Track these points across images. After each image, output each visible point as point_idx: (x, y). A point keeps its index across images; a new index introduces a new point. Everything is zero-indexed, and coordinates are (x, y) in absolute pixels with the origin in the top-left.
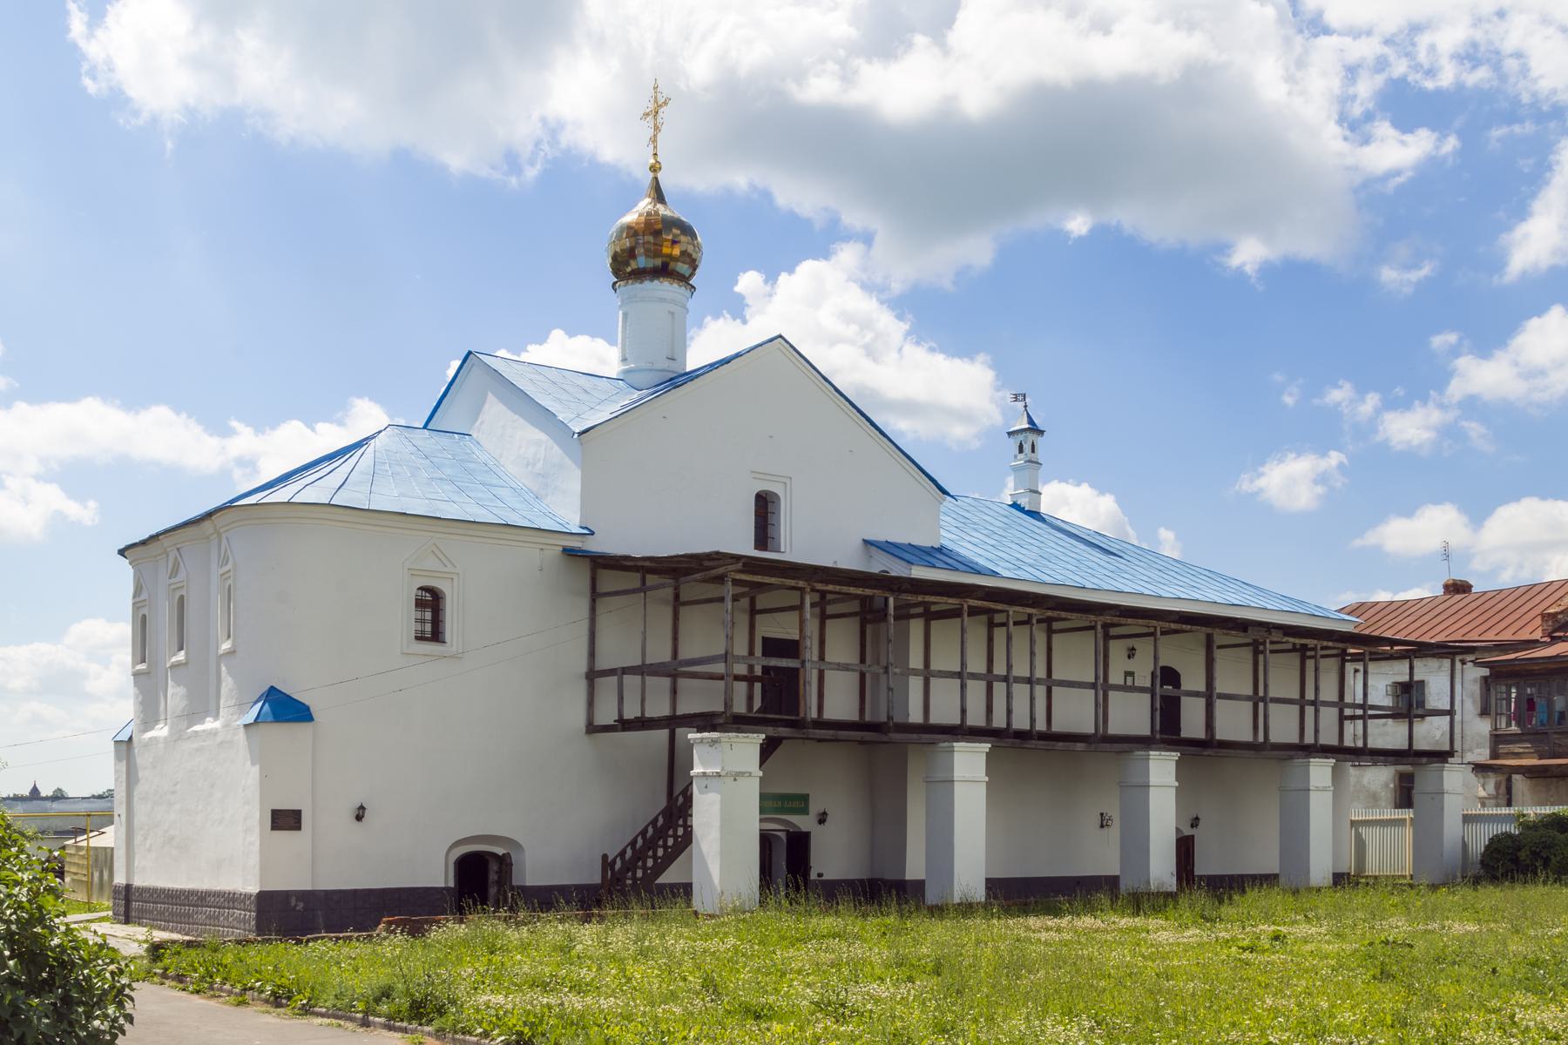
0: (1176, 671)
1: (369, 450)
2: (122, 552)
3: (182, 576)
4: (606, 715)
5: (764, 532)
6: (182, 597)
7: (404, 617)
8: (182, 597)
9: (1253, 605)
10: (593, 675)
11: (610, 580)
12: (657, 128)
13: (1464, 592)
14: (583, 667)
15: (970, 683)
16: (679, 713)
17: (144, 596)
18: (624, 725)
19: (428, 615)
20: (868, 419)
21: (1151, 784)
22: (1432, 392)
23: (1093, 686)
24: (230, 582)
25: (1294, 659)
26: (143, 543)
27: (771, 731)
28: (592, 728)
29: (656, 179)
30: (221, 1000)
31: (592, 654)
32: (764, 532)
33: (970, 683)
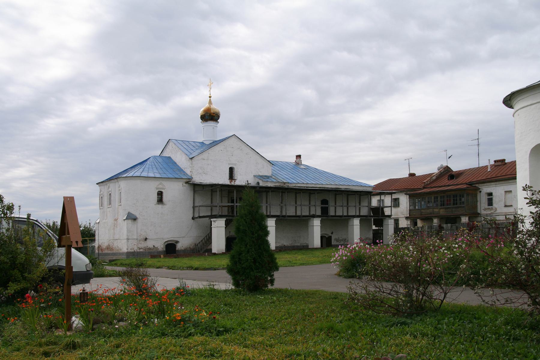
0: (506, 106)
1: (148, 162)
2: (97, 184)
3: (110, 189)
4: (197, 215)
5: (231, 176)
6: (110, 194)
7: (155, 197)
8: (110, 194)
9: (346, 184)
10: (194, 207)
11: (197, 188)
12: (210, 89)
13: (414, 176)
14: (192, 206)
15: (344, 207)
16: (213, 214)
17: (102, 193)
18: (200, 217)
19: (160, 196)
20: (255, 151)
21: (314, 225)
22: (233, 287)
23: (368, 206)
24: (120, 191)
25: (314, 207)
26: (102, 182)
27: (228, 218)
28: (193, 218)
29: (210, 99)
30: (202, 245)
31: (194, 203)
32: (231, 176)
33: (344, 207)
